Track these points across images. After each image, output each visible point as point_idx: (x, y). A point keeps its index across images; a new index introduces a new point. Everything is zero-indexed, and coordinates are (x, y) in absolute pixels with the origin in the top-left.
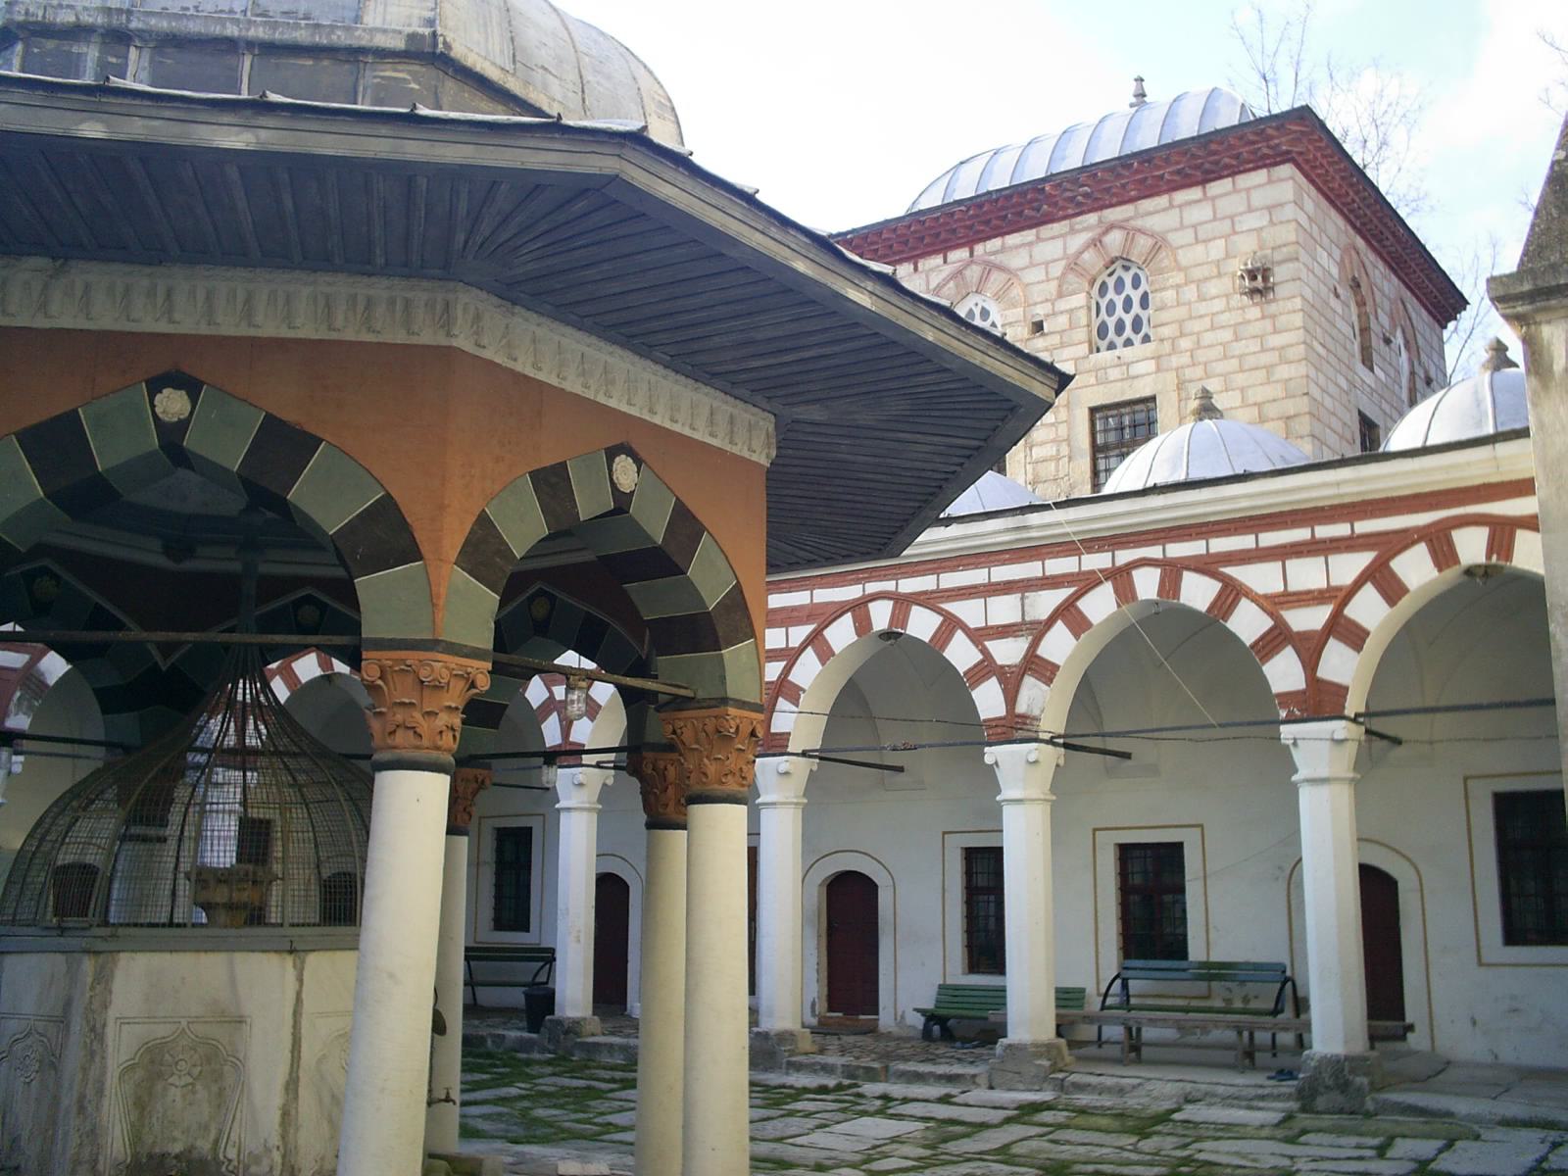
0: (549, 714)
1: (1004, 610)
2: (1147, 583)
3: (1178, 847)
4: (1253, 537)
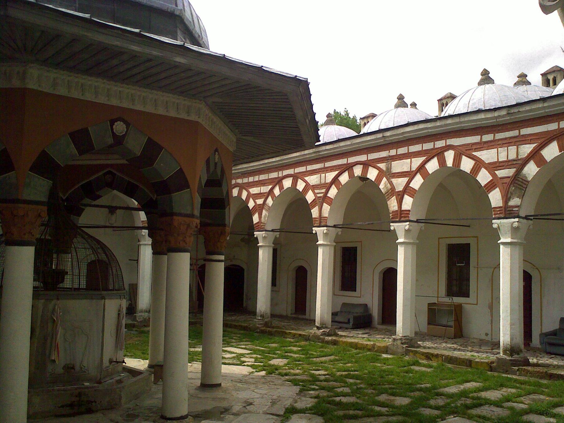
0: (249, 199)
1: (503, 154)
2: (450, 156)
3: (468, 245)
4: (395, 150)
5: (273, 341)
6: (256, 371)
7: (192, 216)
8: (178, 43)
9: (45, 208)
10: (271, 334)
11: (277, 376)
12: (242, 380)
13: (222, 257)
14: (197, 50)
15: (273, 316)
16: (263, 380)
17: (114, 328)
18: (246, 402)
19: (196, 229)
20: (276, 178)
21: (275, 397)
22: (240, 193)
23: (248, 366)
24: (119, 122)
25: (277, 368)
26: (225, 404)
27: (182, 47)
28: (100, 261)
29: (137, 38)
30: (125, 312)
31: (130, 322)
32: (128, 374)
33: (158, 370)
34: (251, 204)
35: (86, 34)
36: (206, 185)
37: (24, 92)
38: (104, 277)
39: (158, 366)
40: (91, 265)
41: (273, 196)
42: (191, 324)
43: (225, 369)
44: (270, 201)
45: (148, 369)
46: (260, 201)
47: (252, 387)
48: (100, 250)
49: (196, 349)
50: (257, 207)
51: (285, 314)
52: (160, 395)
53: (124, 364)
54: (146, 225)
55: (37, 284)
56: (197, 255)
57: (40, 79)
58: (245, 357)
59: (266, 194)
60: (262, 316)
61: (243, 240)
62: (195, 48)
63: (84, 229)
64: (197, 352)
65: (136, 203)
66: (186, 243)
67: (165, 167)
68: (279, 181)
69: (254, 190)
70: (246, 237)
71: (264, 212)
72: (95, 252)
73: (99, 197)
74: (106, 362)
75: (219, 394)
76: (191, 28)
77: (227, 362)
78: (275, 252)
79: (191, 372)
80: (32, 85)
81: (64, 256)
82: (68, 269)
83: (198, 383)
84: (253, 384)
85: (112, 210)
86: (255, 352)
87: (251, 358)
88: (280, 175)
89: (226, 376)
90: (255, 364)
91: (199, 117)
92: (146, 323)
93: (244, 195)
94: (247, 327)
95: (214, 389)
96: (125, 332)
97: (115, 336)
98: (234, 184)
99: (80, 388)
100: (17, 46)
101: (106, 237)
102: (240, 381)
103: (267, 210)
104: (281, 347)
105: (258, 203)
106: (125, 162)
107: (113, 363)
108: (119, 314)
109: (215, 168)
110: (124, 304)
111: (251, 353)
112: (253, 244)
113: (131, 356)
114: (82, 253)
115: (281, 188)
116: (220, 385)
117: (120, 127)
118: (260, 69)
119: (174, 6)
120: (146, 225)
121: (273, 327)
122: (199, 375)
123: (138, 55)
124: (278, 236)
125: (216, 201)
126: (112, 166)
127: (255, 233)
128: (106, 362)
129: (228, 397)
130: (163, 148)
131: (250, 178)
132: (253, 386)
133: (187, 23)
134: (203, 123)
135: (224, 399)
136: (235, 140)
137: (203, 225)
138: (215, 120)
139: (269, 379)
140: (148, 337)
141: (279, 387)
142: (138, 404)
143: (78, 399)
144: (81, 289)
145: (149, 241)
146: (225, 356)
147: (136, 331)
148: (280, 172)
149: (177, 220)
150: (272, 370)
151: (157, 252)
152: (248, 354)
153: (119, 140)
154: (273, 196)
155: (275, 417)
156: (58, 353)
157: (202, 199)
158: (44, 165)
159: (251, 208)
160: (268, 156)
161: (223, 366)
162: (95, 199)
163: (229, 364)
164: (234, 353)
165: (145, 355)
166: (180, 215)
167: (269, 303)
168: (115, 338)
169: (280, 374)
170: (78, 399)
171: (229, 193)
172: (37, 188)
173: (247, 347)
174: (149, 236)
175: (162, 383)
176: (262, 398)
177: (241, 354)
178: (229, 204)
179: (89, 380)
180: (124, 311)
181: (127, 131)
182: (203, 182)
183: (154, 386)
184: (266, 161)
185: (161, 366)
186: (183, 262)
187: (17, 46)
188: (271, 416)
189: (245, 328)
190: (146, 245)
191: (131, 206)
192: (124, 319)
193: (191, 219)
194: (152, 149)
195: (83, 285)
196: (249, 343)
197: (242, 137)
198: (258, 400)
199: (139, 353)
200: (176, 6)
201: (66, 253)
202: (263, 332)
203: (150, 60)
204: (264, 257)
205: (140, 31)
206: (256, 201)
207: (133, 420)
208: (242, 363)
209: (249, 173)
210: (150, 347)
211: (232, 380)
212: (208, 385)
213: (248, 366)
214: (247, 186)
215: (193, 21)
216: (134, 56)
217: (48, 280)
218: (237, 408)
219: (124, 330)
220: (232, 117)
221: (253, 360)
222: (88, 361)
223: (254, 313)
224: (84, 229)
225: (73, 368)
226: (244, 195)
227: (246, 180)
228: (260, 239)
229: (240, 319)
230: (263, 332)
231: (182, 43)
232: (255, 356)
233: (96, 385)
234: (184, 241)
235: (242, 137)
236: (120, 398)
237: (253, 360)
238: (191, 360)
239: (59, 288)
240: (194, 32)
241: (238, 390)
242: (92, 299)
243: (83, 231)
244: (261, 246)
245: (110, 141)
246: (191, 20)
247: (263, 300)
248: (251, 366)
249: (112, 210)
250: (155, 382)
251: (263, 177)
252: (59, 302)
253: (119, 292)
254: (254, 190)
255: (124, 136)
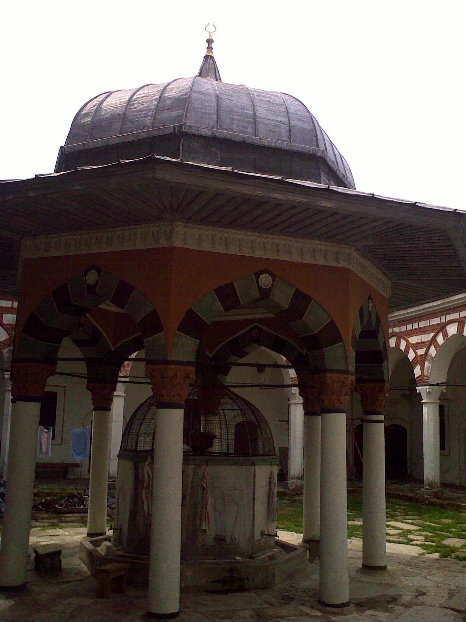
5: (445, 515)
6: (428, 553)
7: (347, 372)
8: (323, 186)
9: (193, 369)
10: (442, 506)
11: (453, 560)
12: (411, 563)
13: (382, 418)
14: (343, 191)
15: (443, 485)
16: (437, 565)
17: (265, 497)
18: (417, 591)
19: (351, 386)
20: (439, 324)
21: (452, 587)
22: (398, 343)
23: (417, 545)
24: (264, 275)
25: (453, 550)
26: (391, 592)
27: (328, 190)
28: (249, 423)
29: (280, 186)
30: (276, 479)
31: (282, 490)
32: (281, 549)
33: (314, 546)
34: (411, 355)
35: (228, 187)
36: (360, 337)
37: (170, 250)
38: (253, 441)
39: (312, 541)
40: (239, 427)
41: (437, 346)
42: (349, 492)
43: (391, 548)
44: (433, 351)
45: (302, 544)
46: (421, 352)
47: (424, 572)
48: (248, 412)
49: (356, 523)
50: (419, 358)
51: (458, 482)
52: (317, 576)
53: (276, 538)
54: (297, 383)
55: (187, 447)
56: (352, 415)
57: (186, 236)
58: (412, 534)
59: (428, 343)
60: (431, 485)
61: (404, 396)
62: (340, 189)
63: (232, 389)
64: (356, 525)
65: (285, 359)
66: (341, 403)
67: (314, 319)
68: (442, 328)
69: (414, 340)
70: (408, 393)
71: (427, 364)
72: (243, 413)
73: (246, 354)
74: (257, 535)
75: (383, 578)
76: (335, 168)
77: (391, 539)
78: (442, 409)
79: (351, 550)
80: (178, 243)
81: (211, 418)
82: (217, 432)
83: (360, 563)
84: (426, 568)
85: (261, 368)
86: (425, 528)
87: (421, 535)
88: (443, 321)
89: (391, 557)
90: (426, 543)
91: (349, 264)
92: (299, 491)
93: (403, 345)
94: (413, 497)
95: (378, 572)
96: (277, 500)
97: (266, 506)
98: (391, 333)
99: (231, 563)
100: (164, 206)
101: (252, 396)
102: (409, 564)
103: (429, 362)
104: (456, 523)
105: (419, 354)
106: (271, 315)
107: (265, 536)
108: (270, 482)
109: (370, 318)
110: (276, 470)
111: (419, 530)
112: (415, 400)
113: (283, 528)
114: (230, 414)
115: (445, 335)
116: (385, 568)
117: (265, 280)
118: (414, 206)
119: (315, 148)
120: (297, 383)
121: (445, 499)
122: (360, 555)
123: (281, 202)
124: (444, 391)
125: (372, 353)
126: (259, 320)
127: (417, 388)
128: (257, 535)
129: (395, 583)
130: (312, 299)
131: (408, 326)
132: (425, 571)
133: (330, 163)
134: (354, 269)
135: (391, 585)
136: (390, 286)
137: (358, 381)
138: (366, 264)
139: (443, 563)
140: (301, 507)
141: (457, 574)
142: (293, 585)
143: (229, 574)
144: (230, 454)
145: (300, 400)
146: (388, 532)
147: (288, 500)
148: (443, 318)
149: (331, 378)
150: (447, 553)
151: (309, 412)
152: (416, 531)
153: (265, 293)
154: (437, 346)
155: (455, 613)
156: (209, 523)
157: (357, 353)
158: (192, 324)
159: (411, 360)
160: (428, 301)
161: (387, 544)
162: (241, 357)
163: (394, 542)
164: (399, 529)
165: (298, 528)
166: (333, 371)
167: (438, 472)
168: (266, 509)
169: (457, 558)
170: (229, 574)
171: (386, 344)
172: (185, 348)
173: (415, 522)
174: (301, 394)
175: (318, 561)
176: (438, 587)
177: (408, 530)
178: (387, 358)
179: (240, 555)
180: (276, 477)
181: (272, 285)
182: (357, 334)
183: (310, 565)
184: (426, 306)
185: (317, 542)
186: (339, 423)
187: (164, 206)
188: (450, 612)
189: (410, 499)
190: (296, 404)
191: (279, 364)
192: (276, 488)
193: (346, 376)
194: (301, 300)
195: (232, 450)
196: (417, 517)
197: (398, 282)
198: (432, 589)
199: (292, 525)
200: (318, 147)
201: (214, 414)
202: (432, 504)
203: (294, 207)
204: (429, 415)
205: (283, 178)
206: (417, 351)
207: (288, 604)
208: (409, 542)
209: (406, 320)
210: (304, 519)
211: (399, 563)
212: (371, 567)
213: (417, 545)
214: (406, 335)
215: (336, 160)
216: (278, 204)
217: (197, 445)
218: (407, 598)
219: (276, 499)
220: (385, 261)
221: (423, 538)
222: (239, 533)
223: (421, 481)
224: (230, 389)
225: (224, 540)
226: (403, 345)
227: (403, 329)
228: (424, 395)
229: (405, 488)
230: (432, 504)
231: (326, 186)
232: (425, 533)
233: (248, 560)
234: (339, 400)
235: (398, 282)
236: (274, 576)
237: (423, 538)
238: (350, 536)
239: (207, 452)
240: (338, 172)
241: (407, 574)
242: (242, 465)
243: (230, 391)
244: (425, 403)
245: (257, 295)
246: (334, 160)
247: (431, 467)
248: (421, 546)
249: (261, 368)
250: (311, 560)
251: (423, 324)
252: (208, 468)
253: (270, 457)
254: (414, 340)
255: (270, 288)
